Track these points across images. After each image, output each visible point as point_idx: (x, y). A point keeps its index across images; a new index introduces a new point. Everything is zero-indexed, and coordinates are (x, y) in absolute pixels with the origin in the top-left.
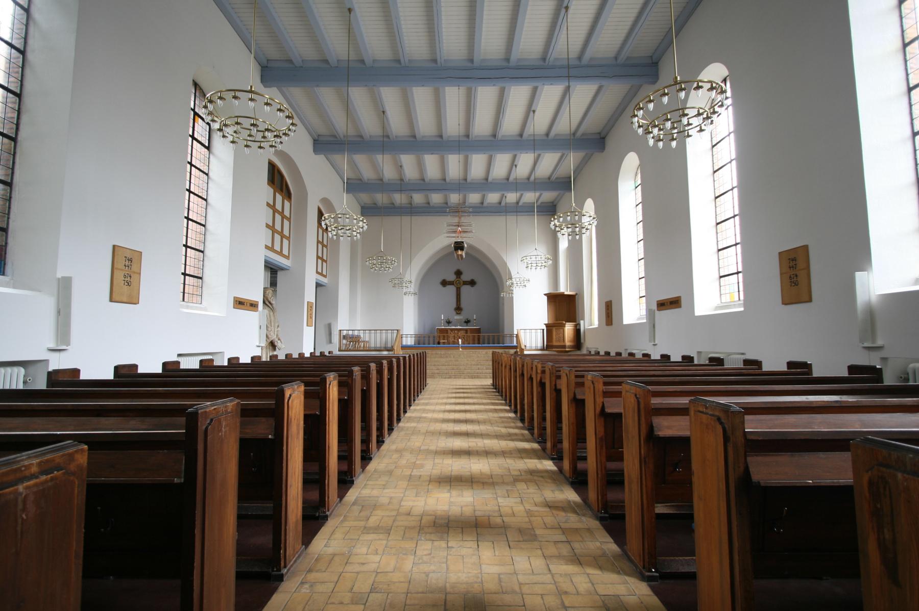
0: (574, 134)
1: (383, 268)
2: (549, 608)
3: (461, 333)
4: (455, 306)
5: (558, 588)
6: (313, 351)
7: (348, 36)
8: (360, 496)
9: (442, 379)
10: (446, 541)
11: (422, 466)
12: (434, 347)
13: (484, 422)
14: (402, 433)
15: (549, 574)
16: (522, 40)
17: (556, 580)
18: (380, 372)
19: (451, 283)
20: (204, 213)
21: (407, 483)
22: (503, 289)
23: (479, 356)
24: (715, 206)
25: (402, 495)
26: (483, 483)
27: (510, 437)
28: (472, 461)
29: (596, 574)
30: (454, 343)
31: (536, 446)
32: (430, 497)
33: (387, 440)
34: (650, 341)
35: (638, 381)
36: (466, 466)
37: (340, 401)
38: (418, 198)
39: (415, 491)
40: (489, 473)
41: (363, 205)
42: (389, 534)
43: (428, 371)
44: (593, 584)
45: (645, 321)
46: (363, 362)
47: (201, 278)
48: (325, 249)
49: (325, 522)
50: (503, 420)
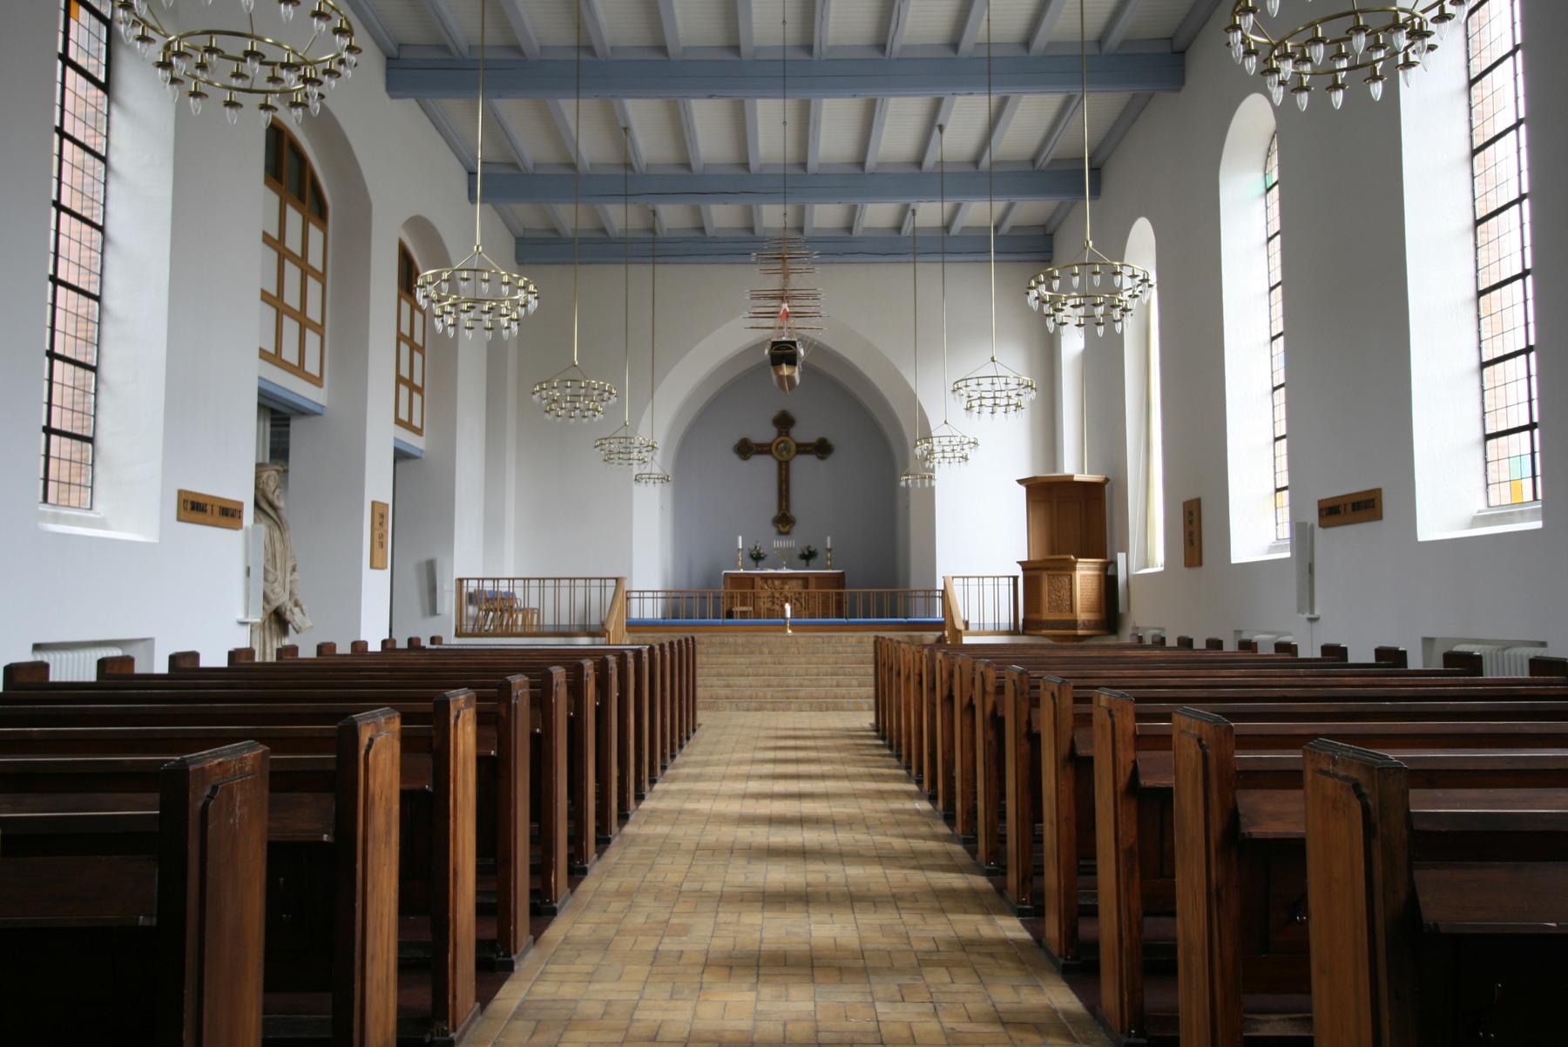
0: (1100, 42)
1: (578, 411)
3: (792, 588)
4: (773, 511)
6: (387, 637)
8: (530, 998)
9: (738, 713)
11: (684, 930)
13: (849, 823)
14: (633, 851)
19: (763, 449)
20: (96, 264)
21: (648, 968)
22: (906, 465)
23: (841, 649)
24: (1476, 245)
28: (813, 918)
30: (771, 613)
31: (981, 882)
33: (595, 868)
34: (1300, 610)
35: (1333, 732)
37: (481, 760)
38: (672, 216)
39: (668, 987)
40: (855, 944)
43: (699, 691)
45: (1287, 555)
46: (536, 665)
47: (90, 440)
48: (418, 357)
49: (607, 847)
50: (898, 821)
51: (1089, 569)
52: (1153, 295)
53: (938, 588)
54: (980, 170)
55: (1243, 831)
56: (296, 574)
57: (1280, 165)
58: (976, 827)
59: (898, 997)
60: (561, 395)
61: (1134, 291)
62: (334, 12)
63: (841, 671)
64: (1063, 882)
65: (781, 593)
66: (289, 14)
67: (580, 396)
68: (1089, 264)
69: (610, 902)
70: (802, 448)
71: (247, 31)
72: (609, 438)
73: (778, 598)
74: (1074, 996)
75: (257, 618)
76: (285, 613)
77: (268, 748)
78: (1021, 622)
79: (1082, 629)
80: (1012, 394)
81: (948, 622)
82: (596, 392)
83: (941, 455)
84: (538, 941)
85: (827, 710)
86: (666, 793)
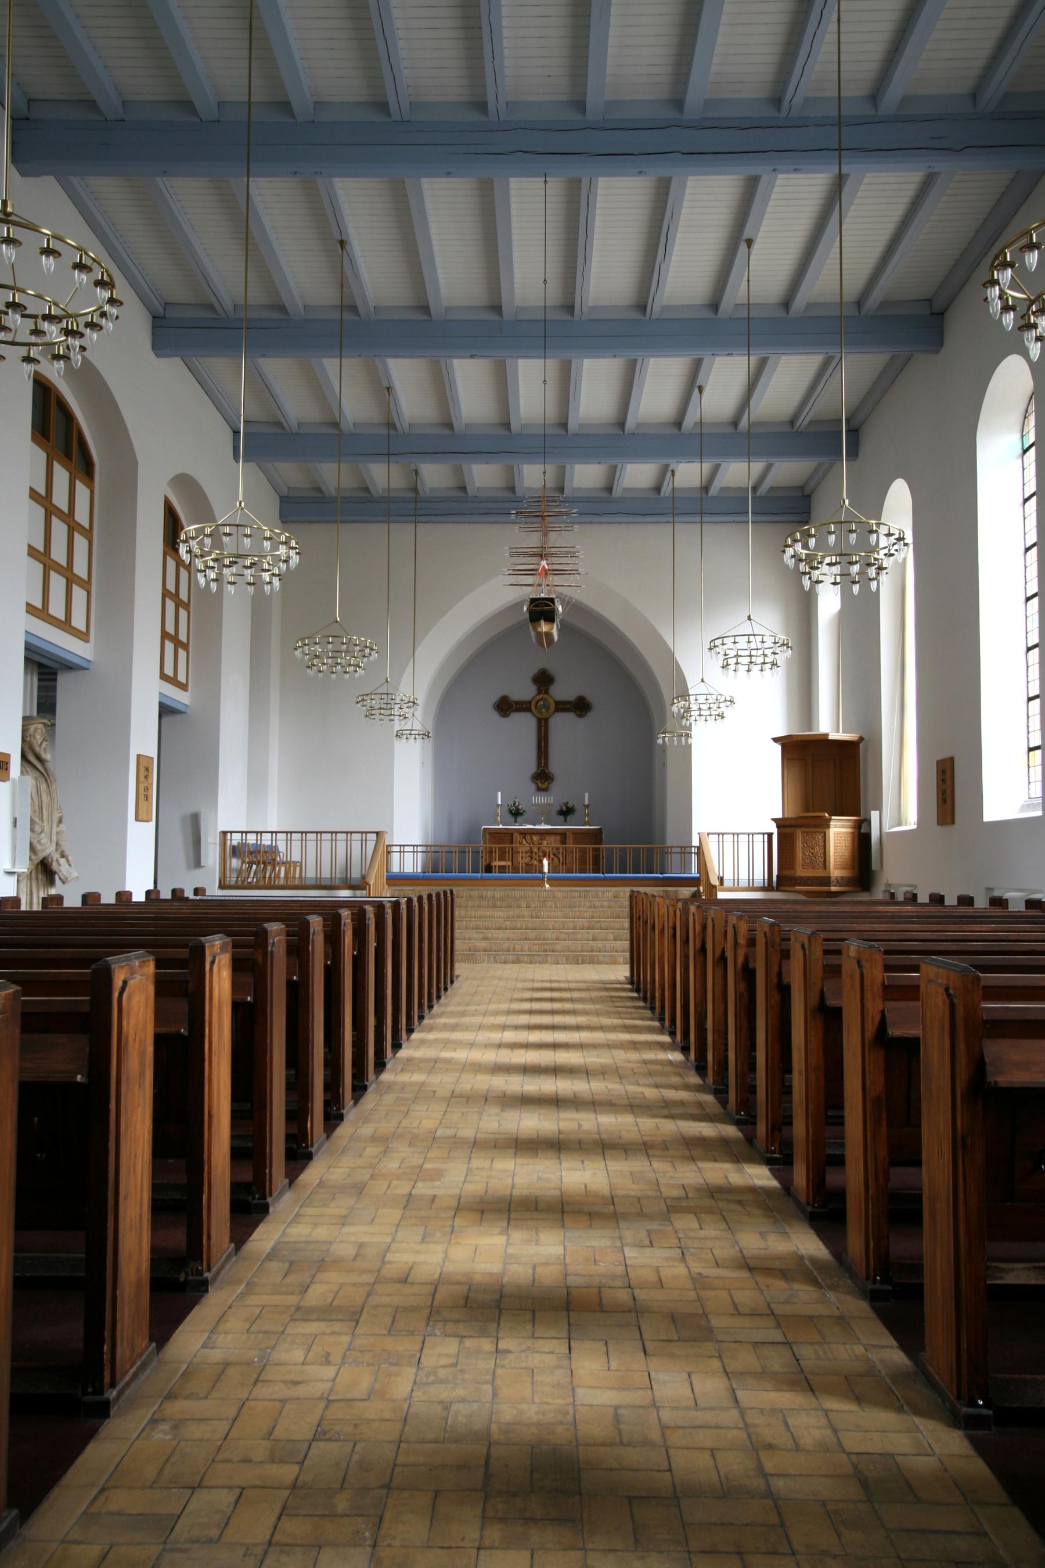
0: (859, 303)
2: (726, 1476)
4: (532, 768)
5: (753, 1436)
6: (151, 887)
7: (248, 46)
10: (495, 1340)
11: (437, 1175)
12: (476, 879)
13: (603, 1072)
14: (389, 1098)
15: (735, 1407)
16: (718, 50)
17: (749, 1421)
18: (333, 938)
19: (523, 707)
21: (401, 1212)
22: (663, 721)
25: (389, 1240)
26: (591, 1215)
27: (667, 1109)
29: (844, 1411)
30: (529, 868)
31: (731, 1131)
32: (458, 1243)
33: (352, 1114)
36: (549, 1176)
37: (237, 1006)
39: (420, 1230)
41: (285, 491)
42: (357, 1322)
43: (458, 944)
44: (835, 1431)
50: (650, 1071)
51: (843, 827)
52: (909, 554)
53: (693, 845)
54: (738, 431)
55: (989, 1080)
56: (61, 825)
57: (1037, 426)
58: (727, 1078)
59: (647, 1242)
60: (323, 651)
61: (889, 550)
62: (95, 264)
63: (598, 925)
64: (811, 1131)
65: (539, 848)
66: (51, 265)
67: (342, 652)
68: (845, 522)
69: (365, 1147)
70: (561, 706)
71: (11, 283)
72: (371, 694)
73: (536, 853)
74: (820, 1244)
75: (23, 868)
76: (51, 864)
77: (19, 988)
78: (775, 878)
79: (835, 886)
80: (768, 652)
81: (703, 878)
82: (358, 648)
83: (698, 713)
84: (293, 1185)
85: (583, 962)
86: (423, 1042)
